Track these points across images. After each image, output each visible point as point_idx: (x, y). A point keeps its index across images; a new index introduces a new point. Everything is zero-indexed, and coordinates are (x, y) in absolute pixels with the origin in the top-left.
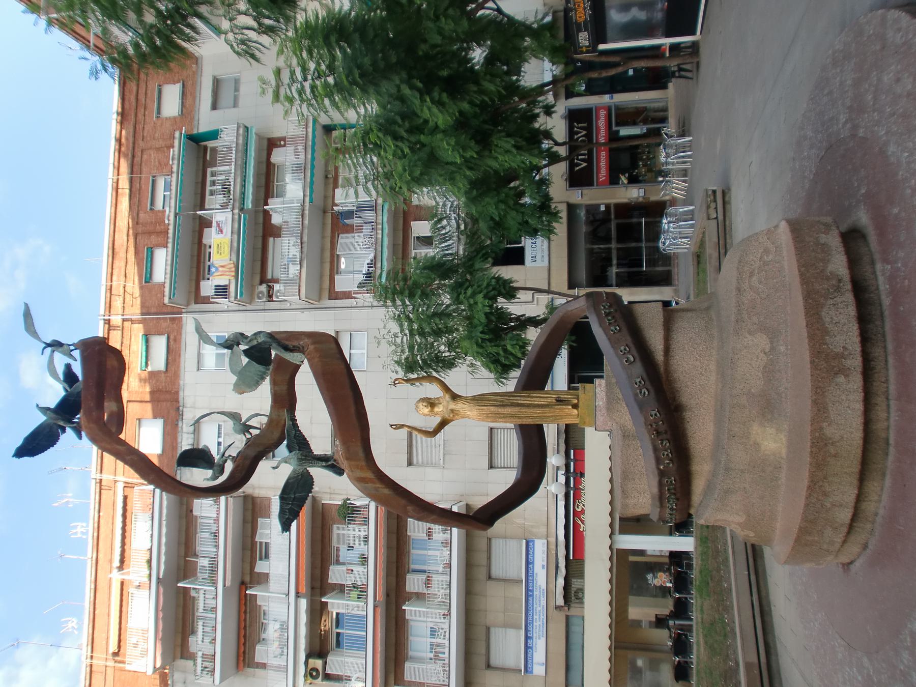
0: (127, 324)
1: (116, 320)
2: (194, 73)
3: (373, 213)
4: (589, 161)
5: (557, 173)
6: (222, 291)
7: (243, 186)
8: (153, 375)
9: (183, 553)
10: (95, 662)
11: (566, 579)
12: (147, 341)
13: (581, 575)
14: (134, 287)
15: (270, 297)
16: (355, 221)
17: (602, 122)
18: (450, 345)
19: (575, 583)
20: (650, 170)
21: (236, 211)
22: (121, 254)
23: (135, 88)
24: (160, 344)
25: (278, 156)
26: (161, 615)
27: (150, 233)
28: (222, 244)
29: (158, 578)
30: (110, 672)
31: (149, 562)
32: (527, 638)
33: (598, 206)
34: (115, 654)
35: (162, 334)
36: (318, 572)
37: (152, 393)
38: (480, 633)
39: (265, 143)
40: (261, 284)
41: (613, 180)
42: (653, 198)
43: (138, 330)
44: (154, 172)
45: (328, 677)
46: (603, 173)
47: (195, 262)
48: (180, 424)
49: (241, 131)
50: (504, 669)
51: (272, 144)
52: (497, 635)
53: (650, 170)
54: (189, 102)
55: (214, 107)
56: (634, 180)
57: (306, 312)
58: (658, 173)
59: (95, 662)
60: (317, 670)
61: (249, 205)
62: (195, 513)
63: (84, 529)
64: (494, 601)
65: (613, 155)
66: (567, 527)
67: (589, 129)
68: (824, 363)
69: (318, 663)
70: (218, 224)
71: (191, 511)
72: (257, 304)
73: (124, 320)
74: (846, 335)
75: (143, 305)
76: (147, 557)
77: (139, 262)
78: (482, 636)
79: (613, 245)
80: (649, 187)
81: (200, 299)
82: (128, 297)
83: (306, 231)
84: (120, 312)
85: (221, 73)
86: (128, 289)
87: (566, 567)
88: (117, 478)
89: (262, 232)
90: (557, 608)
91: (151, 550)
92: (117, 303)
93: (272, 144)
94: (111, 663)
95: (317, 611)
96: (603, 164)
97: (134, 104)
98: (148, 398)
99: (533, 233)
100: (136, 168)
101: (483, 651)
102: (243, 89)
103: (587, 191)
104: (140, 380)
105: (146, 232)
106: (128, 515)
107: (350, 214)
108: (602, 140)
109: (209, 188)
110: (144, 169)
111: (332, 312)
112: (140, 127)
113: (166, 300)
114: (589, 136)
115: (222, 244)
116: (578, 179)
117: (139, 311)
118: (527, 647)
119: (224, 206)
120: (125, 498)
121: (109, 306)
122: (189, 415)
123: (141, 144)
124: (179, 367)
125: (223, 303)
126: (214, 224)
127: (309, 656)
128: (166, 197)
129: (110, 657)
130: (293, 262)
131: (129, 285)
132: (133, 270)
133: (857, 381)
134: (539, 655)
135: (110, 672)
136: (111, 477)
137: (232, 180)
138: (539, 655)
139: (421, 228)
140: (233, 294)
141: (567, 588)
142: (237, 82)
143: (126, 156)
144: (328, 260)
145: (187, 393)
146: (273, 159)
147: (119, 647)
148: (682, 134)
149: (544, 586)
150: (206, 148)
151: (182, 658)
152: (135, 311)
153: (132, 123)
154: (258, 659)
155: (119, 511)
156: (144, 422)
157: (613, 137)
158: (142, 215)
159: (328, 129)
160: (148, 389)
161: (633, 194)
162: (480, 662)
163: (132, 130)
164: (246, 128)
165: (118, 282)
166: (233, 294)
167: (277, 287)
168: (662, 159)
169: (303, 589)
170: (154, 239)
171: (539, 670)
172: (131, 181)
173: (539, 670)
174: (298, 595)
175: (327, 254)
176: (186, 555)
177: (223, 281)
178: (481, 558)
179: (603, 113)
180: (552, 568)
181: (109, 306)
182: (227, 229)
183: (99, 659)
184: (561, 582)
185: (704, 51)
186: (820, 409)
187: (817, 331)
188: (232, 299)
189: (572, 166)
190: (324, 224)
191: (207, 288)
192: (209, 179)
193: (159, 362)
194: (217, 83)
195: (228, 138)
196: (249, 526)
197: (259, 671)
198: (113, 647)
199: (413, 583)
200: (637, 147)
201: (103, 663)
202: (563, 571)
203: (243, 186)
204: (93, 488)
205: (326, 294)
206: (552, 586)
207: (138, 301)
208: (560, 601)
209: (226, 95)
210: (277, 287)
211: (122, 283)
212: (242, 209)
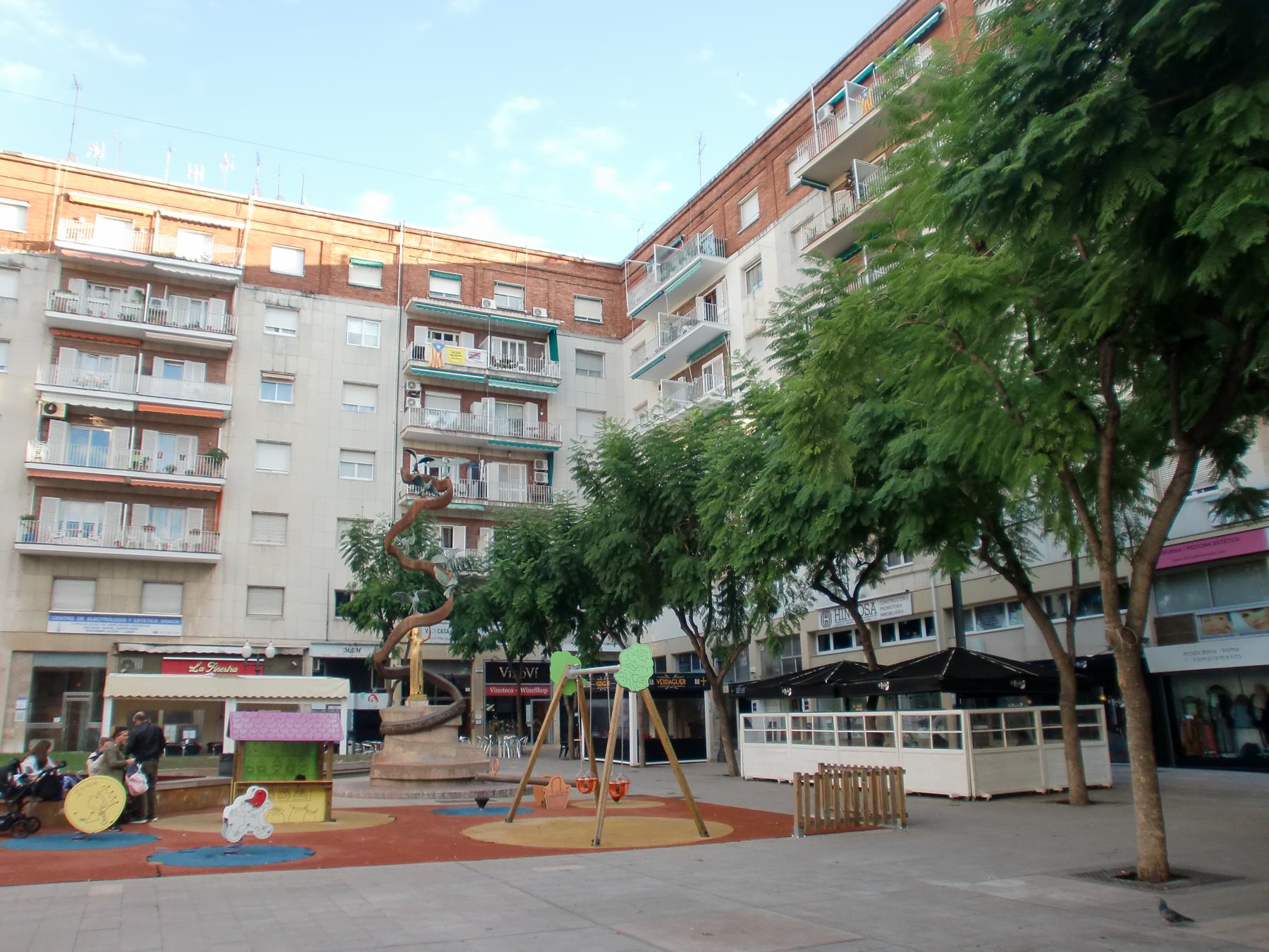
0: (394, 249)
1: (399, 238)
2: (610, 337)
3: (476, 496)
4: (507, 680)
5: (500, 655)
6: (419, 353)
7: (508, 380)
8: (344, 269)
9: (172, 282)
10: (59, 173)
11: (144, 654)
12: (377, 267)
13: (145, 670)
14: (428, 259)
15: (411, 394)
16: (470, 480)
17: (537, 690)
18: (372, 569)
19: (139, 662)
20: (497, 729)
21: (487, 373)
22: (460, 250)
23: (601, 277)
24: (372, 280)
25: (531, 409)
26: (117, 261)
27: (474, 280)
28: (461, 355)
29: (153, 263)
30: (48, 189)
31: (171, 256)
32: (86, 616)
33: (469, 686)
34: (67, 198)
35: (382, 284)
36: (152, 419)
37: (329, 267)
38: (91, 571)
39: (544, 398)
40: (422, 385)
41: (490, 699)
42: (473, 732)
43: (388, 259)
44: (528, 289)
45: (45, 421)
46: (497, 690)
47: (446, 325)
48: (299, 293)
49: (555, 382)
50: (52, 592)
51: (542, 402)
52: (89, 586)
53: (497, 729)
54: (585, 328)
55: (578, 351)
56: (489, 716)
57: (394, 426)
58: (497, 732)
59: (59, 173)
60: (54, 411)
61: (492, 383)
62: (212, 300)
63: (196, 178)
64: (121, 587)
65: (512, 699)
66: (194, 654)
67: (533, 680)
68: (452, 768)
69: (62, 413)
70: (477, 354)
71: (214, 296)
72: (403, 380)
73: (398, 247)
74: (459, 775)
75: (409, 266)
76: (178, 255)
77: (449, 266)
78: (87, 574)
79: (865, 731)
80: (483, 728)
81: (412, 323)
82: (419, 252)
83: (465, 436)
84: (407, 244)
85: (607, 358)
86: (426, 254)
87: (156, 654)
88: (249, 222)
89: (468, 391)
90: (116, 645)
91: (184, 259)
92: (413, 241)
93: (542, 402)
94: (57, 191)
95: (115, 418)
96: (505, 691)
97: (588, 276)
98: (325, 262)
99: (455, 636)
100: (533, 272)
101: (73, 574)
102: (592, 379)
103: (482, 677)
104: (344, 256)
105: (478, 278)
106: (212, 229)
107: (476, 475)
108: (522, 690)
109: (509, 341)
110: (531, 280)
111: (393, 451)
112: (569, 279)
113: (415, 299)
114: (527, 680)
115: (461, 355)
116: (492, 670)
117: (406, 262)
118: (76, 616)
119: (492, 359)
120: (229, 229)
121: (411, 232)
122: (306, 302)
123: (554, 279)
124: (351, 297)
125: (408, 352)
126: (478, 351)
127: (69, 406)
128: (504, 302)
129: (64, 191)
130: (441, 421)
131: (430, 255)
132: (444, 259)
133: (447, 777)
134: (68, 627)
135: (48, 189)
136: (250, 216)
137: (517, 370)
138: (68, 627)
139: (460, 533)
140: (416, 363)
141: (136, 654)
142: (598, 374)
143: (545, 263)
144: (438, 449)
145: (327, 303)
146: (529, 404)
147: (75, 203)
148: (522, 753)
149: (136, 633)
150: (545, 341)
151: (63, 269)
152: (406, 258)
153: (574, 273)
154: (64, 351)
155: (217, 222)
156: (301, 255)
157: (525, 699)
158: (491, 273)
159: (550, 456)
160: (333, 263)
161: (478, 716)
162: (61, 571)
163: (567, 271)
164: (556, 386)
165: (432, 244)
166: (416, 363)
167: (418, 401)
168: (506, 737)
169: (142, 409)
170: (469, 283)
171: (53, 626)
172: (521, 266)
173: (53, 626)
174: (137, 403)
175: (443, 449)
176: (170, 286)
177: (428, 354)
178: (164, 575)
179: (545, 691)
180: (155, 640)
181: (411, 232)
182: (472, 363)
183: (63, 177)
184: (142, 648)
185: (575, 762)
186: (439, 767)
187: (460, 767)
188: (413, 363)
189: (504, 665)
190: (469, 447)
191: (422, 333)
192: (518, 342)
193: (359, 278)
194: (599, 355)
195: (551, 369)
196: (198, 354)
197: (48, 351)
198: (75, 196)
199: (142, 511)
200: (516, 719)
201: (58, 182)
202: (152, 650)
203: (508, 380)
204: (241, 195)
205: (408, 445)
206: (136, 640)
207: (414, 262)
208: (123, 648)
209: (589, 363)
210: (418, 401)
211: (433, 248)
212: (488, 377)
